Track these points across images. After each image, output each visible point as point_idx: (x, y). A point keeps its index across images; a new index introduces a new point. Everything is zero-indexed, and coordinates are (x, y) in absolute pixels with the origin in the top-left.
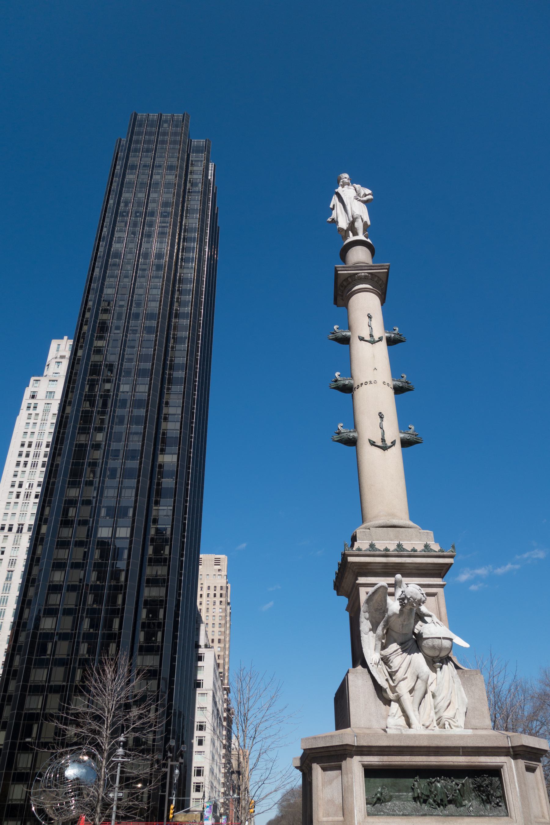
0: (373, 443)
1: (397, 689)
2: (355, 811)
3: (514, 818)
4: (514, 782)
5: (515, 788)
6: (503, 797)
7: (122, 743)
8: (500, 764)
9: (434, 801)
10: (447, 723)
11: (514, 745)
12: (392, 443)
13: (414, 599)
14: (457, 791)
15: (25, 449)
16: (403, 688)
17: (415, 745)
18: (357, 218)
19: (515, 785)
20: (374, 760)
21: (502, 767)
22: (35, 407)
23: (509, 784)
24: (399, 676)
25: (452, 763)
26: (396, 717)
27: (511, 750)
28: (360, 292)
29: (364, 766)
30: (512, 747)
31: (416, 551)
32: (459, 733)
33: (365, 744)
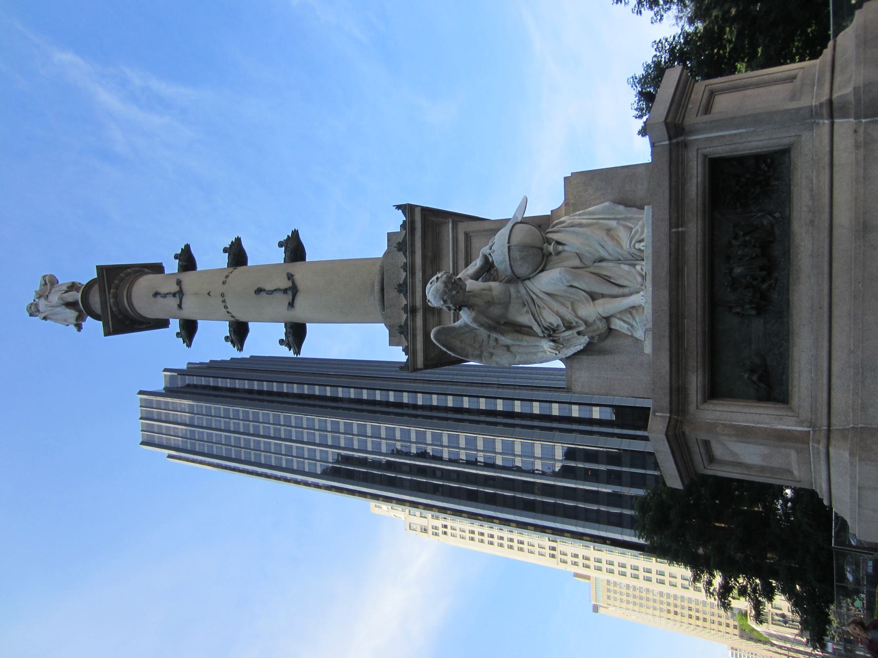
0: (291, 305)
1: (591, 320)
2: (779, 427)
3: (792, 139)
4: (730, 135)
5: (740, 134)
6: (759, 159)
7: (759, 508)
8: (700, 160)
9: (764, 281)
10: (638, 246)
11: (666, 137)
12: (289, 279)
13: (445, 292)
14: (747, 238)
15: (476, 536)
16: (590, 311)
17: (668, 312)
18: (62, 299)
19: (735, 135)
20: (695, 382)
21: (705, 156)
22: (436, 528)
23: (733, 146)
24: (569, 316)
25: (700, 246)
26: (635, 324)
27: (674, 141)
28: (132, 305)
29: (705, 401)
30: (670, 139)
31: (406, 264)
32: (650, 230)
33: (667, 399)
